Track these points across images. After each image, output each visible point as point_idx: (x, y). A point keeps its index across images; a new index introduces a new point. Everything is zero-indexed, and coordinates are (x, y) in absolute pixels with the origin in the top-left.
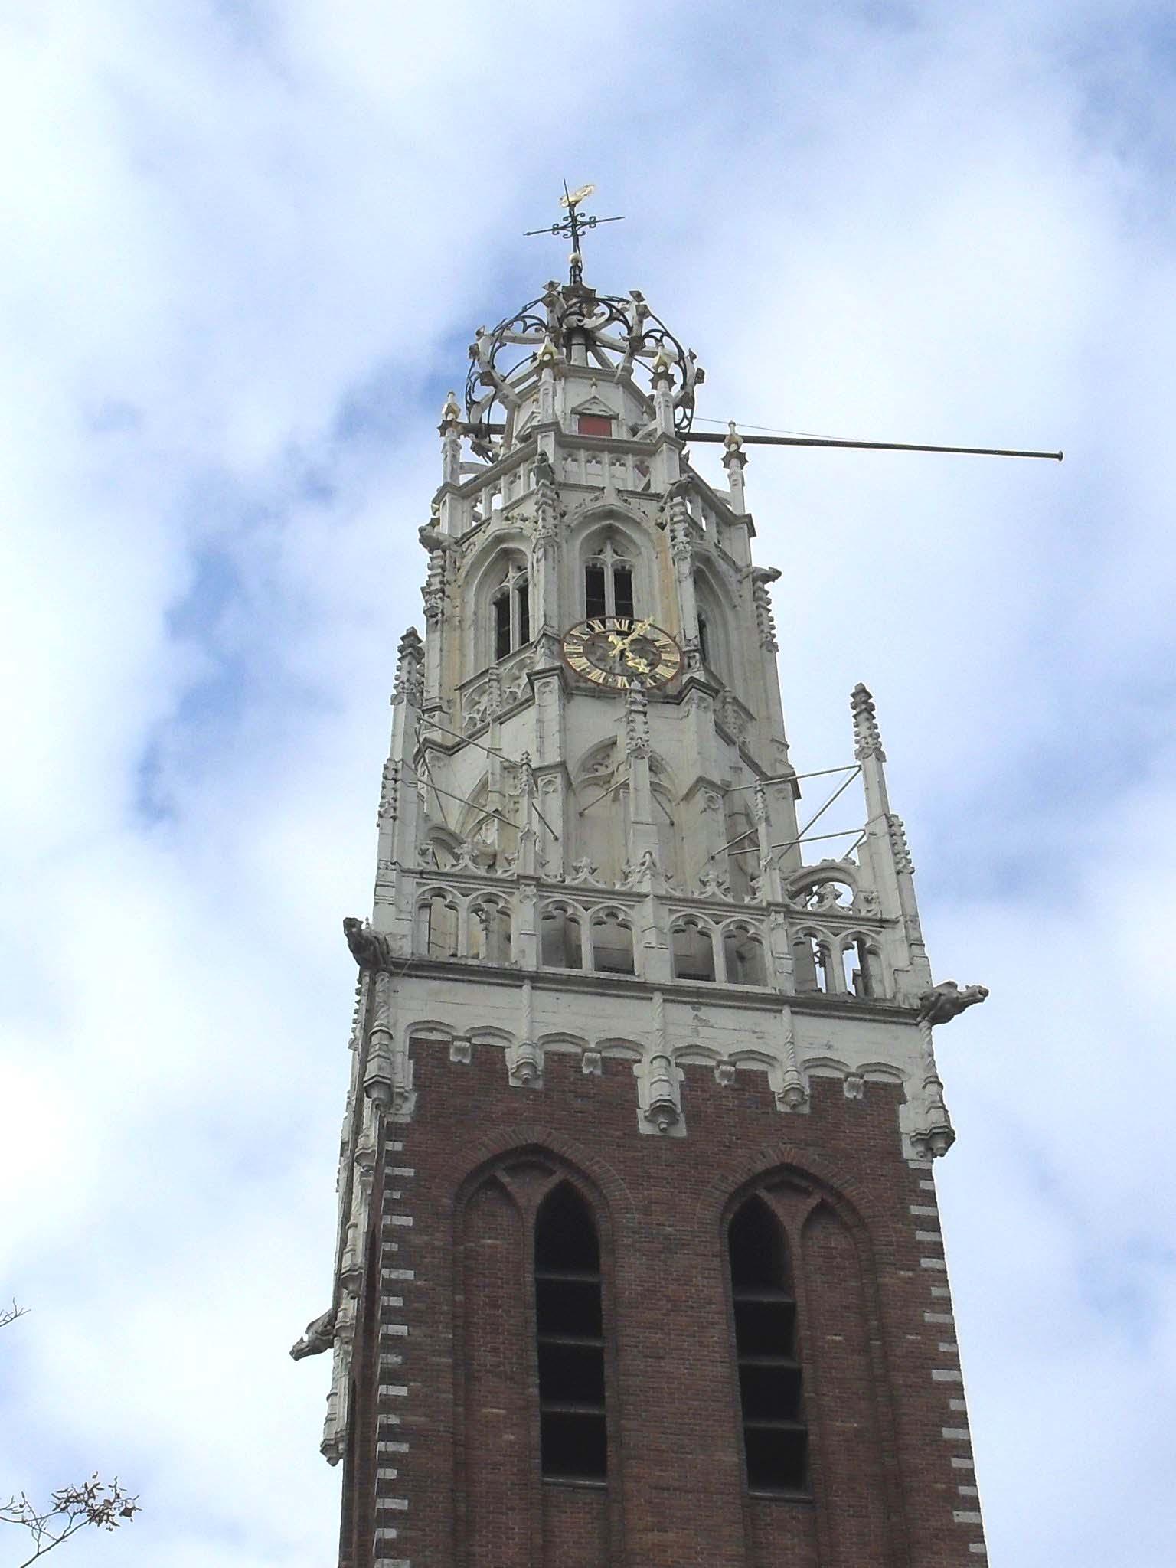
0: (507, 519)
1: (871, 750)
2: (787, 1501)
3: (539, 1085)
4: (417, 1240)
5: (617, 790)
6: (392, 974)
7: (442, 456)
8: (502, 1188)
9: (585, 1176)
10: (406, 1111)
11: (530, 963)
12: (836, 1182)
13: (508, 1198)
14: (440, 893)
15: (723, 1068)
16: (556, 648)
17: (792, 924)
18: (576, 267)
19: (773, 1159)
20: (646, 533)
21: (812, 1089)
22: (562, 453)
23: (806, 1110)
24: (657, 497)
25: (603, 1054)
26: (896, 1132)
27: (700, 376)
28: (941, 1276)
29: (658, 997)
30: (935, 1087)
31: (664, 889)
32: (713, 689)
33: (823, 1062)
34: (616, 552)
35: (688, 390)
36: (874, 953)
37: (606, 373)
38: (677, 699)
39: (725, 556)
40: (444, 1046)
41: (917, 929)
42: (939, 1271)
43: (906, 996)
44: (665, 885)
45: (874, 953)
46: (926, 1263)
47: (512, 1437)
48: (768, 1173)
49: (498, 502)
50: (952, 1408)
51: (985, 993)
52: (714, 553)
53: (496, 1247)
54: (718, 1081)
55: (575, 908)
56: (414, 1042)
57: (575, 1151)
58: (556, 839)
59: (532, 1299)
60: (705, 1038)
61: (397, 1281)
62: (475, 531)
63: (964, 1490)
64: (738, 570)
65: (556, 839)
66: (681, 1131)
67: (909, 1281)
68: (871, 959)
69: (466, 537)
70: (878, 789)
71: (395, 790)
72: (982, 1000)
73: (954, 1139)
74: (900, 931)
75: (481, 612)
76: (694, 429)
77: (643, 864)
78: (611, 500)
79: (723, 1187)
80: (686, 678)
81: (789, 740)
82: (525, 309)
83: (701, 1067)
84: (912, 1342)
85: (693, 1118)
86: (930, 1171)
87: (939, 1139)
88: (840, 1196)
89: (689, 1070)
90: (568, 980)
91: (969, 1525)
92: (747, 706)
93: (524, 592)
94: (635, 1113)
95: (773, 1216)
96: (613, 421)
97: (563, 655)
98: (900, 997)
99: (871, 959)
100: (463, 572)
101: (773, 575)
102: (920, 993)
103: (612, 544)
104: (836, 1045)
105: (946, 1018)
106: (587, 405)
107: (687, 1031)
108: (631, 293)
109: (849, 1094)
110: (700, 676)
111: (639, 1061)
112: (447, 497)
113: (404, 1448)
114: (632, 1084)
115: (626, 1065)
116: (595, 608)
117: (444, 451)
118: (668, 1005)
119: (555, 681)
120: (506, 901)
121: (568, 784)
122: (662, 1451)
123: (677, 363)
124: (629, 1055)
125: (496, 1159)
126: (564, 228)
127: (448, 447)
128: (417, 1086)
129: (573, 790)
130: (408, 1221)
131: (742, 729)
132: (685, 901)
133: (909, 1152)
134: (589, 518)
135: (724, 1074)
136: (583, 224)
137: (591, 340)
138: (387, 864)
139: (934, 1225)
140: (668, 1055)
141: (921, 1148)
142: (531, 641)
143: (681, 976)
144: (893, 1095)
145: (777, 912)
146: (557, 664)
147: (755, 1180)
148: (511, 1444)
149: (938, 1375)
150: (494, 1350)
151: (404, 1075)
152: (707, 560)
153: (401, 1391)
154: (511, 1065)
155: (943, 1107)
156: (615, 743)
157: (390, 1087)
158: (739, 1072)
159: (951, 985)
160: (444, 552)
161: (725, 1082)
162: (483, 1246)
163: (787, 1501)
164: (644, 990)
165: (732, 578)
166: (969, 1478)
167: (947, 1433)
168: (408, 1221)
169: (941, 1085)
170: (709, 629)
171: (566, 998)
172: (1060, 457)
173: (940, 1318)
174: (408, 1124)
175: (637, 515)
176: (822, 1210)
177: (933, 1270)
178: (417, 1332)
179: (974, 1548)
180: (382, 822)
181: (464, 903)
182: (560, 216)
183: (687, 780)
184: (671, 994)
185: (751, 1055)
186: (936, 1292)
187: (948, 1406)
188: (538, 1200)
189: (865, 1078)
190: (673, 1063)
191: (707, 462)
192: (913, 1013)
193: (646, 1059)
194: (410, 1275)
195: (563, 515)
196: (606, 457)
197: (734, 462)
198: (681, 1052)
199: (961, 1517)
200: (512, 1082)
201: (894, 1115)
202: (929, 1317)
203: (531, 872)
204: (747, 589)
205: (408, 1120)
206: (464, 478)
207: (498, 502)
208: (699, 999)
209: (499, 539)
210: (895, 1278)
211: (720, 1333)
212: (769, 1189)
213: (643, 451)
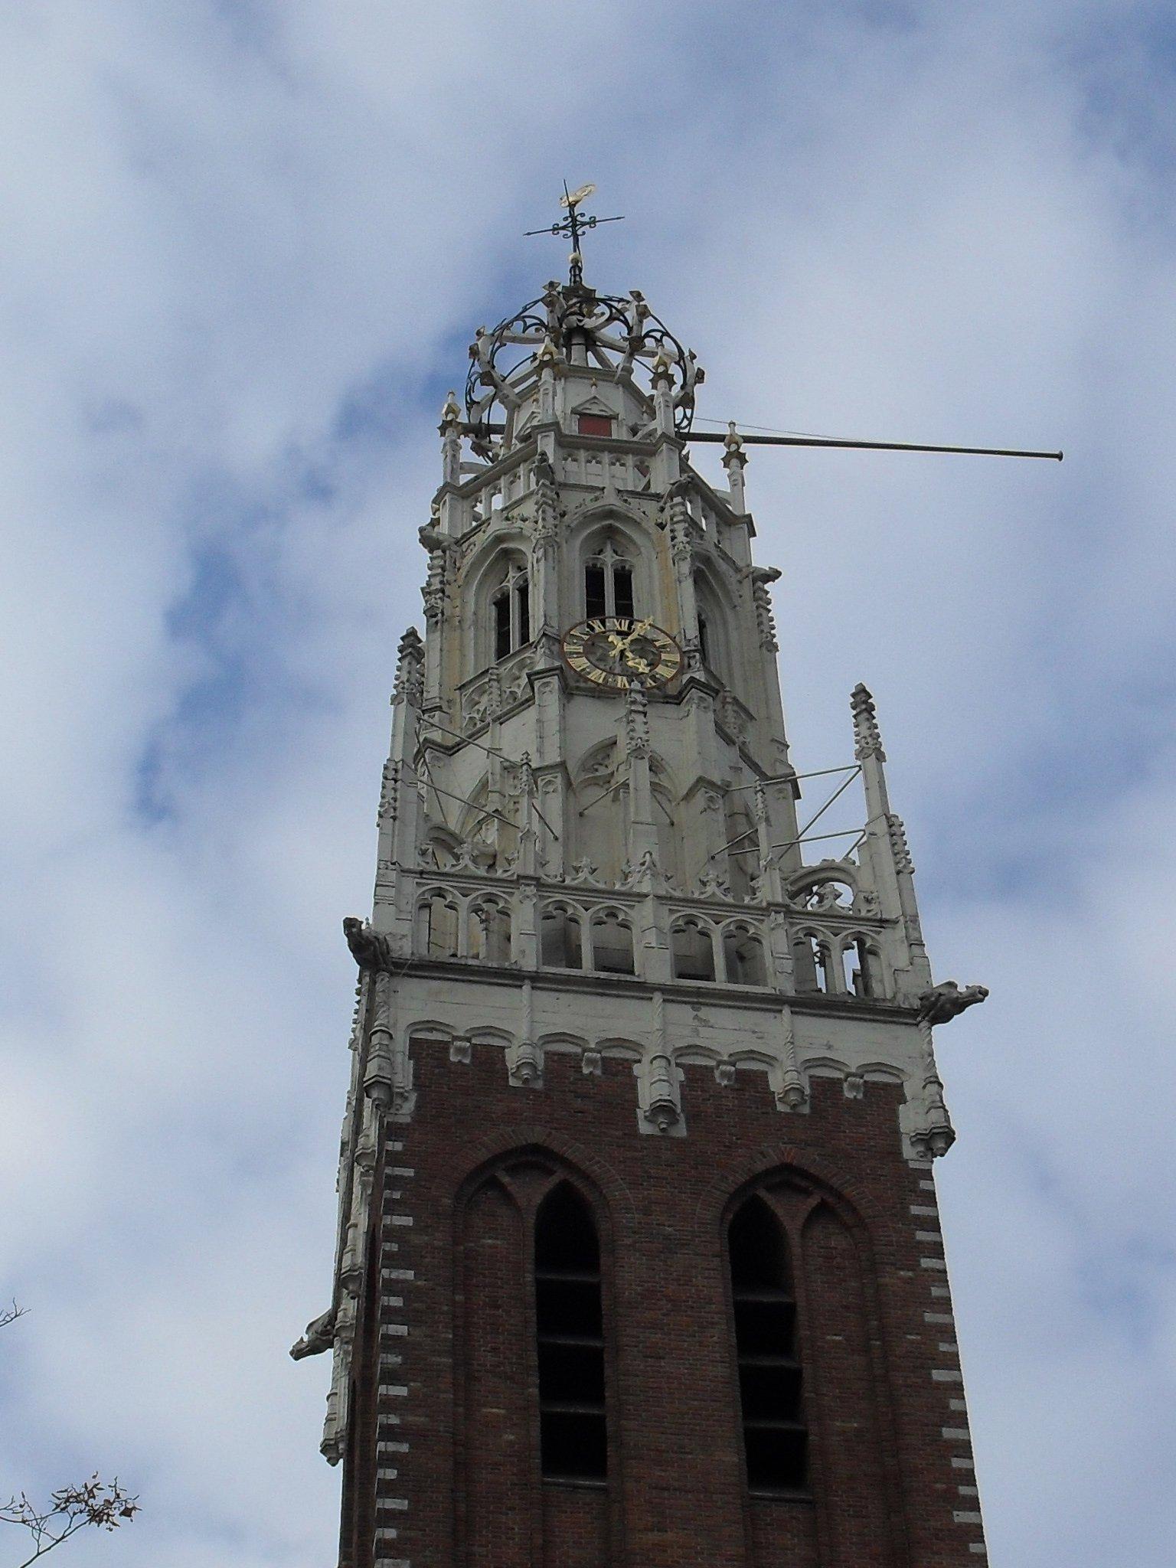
3: (539, 1085)
4: (416, 1240)
5: (617, 790)
6: (392, 974)
7: (442, 456)
8: (501, 1188)
9: (586, 1176)
10: (406, 1111)
11: (530, 963)
12: (835, 1182)
13: (508, 1198)
14: (440, 893)
15: (723, 1068)
16: (556, 648)
17: (792, 924)
18: (576, 267)
19: (774, 1159)
20: (646, 533)
23: (806, 1110)
24: (657, 497)
26: (896, 1132)
27: (700, 376)
28: (941, 1275)
29: (658, 997)
32: (713, 689)
33: (823, 1062)
34: (616, 552)
35: (688, 389)
37: (606, 373)
38: (677, 699)
39: (725, 557)
40: (444, 1047)
41: (918, 929)
42: (939, 1271)
43: (906, 997)
45: (874, 953)
46: (926, 1263)
49: (498, 502)
51: (985, 993)
52: (714, 553)
54: (718, 1081)
55: (575, 908)
57: (575, 1151)
58: (556, 839)
59: (532, 1299)
60: (705, 1038)
61: (397, 1281)
62: (475, 531)
63: (963, 1490)
64: (738, 570)
65: (556, 839)
66: (681, 1131)
68: (870, 959)
69: (466, 537)
70: (878, 789)
71: (395, 790)
72: (982, 1000)
73: (954, 1139)
74: (900, 931)
76: (694, 429)
77: (643, 864)
78: (611, 500)
80: (686, 678)
81: (789, 743)
82: (525, 309)
84: (912, 1342)
85: (693, 1118)
86: (929, 1171)
87: (940, 1138)
88: (839, 1196)
89: (689, 1069)
90: (568, 980)
93: (524, 592)
95: (774, 1215)
96: (613, 421)
97: (563, 655)
98: (900, 997)
99: (870, 959)
100: (463, 572)
101: (773, 575)
102: (920, 992)
105: (946, 1018)
108: (631, 293)
109: (849, 1094)
110: (700, 676)
111: (639, 1061)
112: (447, 497)
113: (404, 1448)
114: (632, 1084)
115: (626, 1065)
116: (595, 608)
117: (444, 451)
118: (669, 1005)
119: (555, 681)
120: (506, 901)
121: (568, 784)
123: (677, 363)
124: (629, 1055)
126: (564, 228)
127: (448, 447)
128: (417, 1086)
130: (408, 1221)
131: (742, 729)
133: (909, 1151)
135: (724, 1074)
136: (583, 224)
137: (590, 340)
138: (387, 864)
139: (934, 1225)
140: (668, 1055)
142: (531, 641)
143: (681, 976)
144: (893, 1095)
145: (777, 912)
146: (557, 664)
147: (755, 1180)
148: (511, 1444)
149: (938, 1375)
151: (404, 1075)
152: (707, 560)
153: (401, 1391)
155: (943, 1107)
156: (615, 743)
157: (389, 1087)
158: (739, 1072)
159: (951, 985)
160: (444, 552)
162: (483, 1246)
164: (643, 990)
165: (732, 578)
166: (969, 1478)
167: (948, 1433)
168: (408, 1221)
169: (941, 1085)
172: (1060, 457)
175: (636, 515)
176: (822, 1211)
177: (933, 1270)
179: (974, 1548)
181: (464, 903)
182: (560, 216)
184: (672, 994)
185: (751, 1055)
186: (936, 1292)
188: (538, 1199)
189: (865, 1078)
190: (673, 1062)
192: (913, 1013)
193: (646, 1059)
194: (410, 1275)
195: (563, 515)
197: (734, 462)
198: (681, 1052)
199: (961, 1517)
200: (512, 1082)
201: (894, 1116)
202: (929, 1317)
203: (531, 872)
204: (747, 590)
205: (408, 1120)
206: (464, 478)
207: (498, 502)
208: (699, 999)
209: (499, 539)
211: (720, 1333)
212: (769, 1189)
213: (643, 451)
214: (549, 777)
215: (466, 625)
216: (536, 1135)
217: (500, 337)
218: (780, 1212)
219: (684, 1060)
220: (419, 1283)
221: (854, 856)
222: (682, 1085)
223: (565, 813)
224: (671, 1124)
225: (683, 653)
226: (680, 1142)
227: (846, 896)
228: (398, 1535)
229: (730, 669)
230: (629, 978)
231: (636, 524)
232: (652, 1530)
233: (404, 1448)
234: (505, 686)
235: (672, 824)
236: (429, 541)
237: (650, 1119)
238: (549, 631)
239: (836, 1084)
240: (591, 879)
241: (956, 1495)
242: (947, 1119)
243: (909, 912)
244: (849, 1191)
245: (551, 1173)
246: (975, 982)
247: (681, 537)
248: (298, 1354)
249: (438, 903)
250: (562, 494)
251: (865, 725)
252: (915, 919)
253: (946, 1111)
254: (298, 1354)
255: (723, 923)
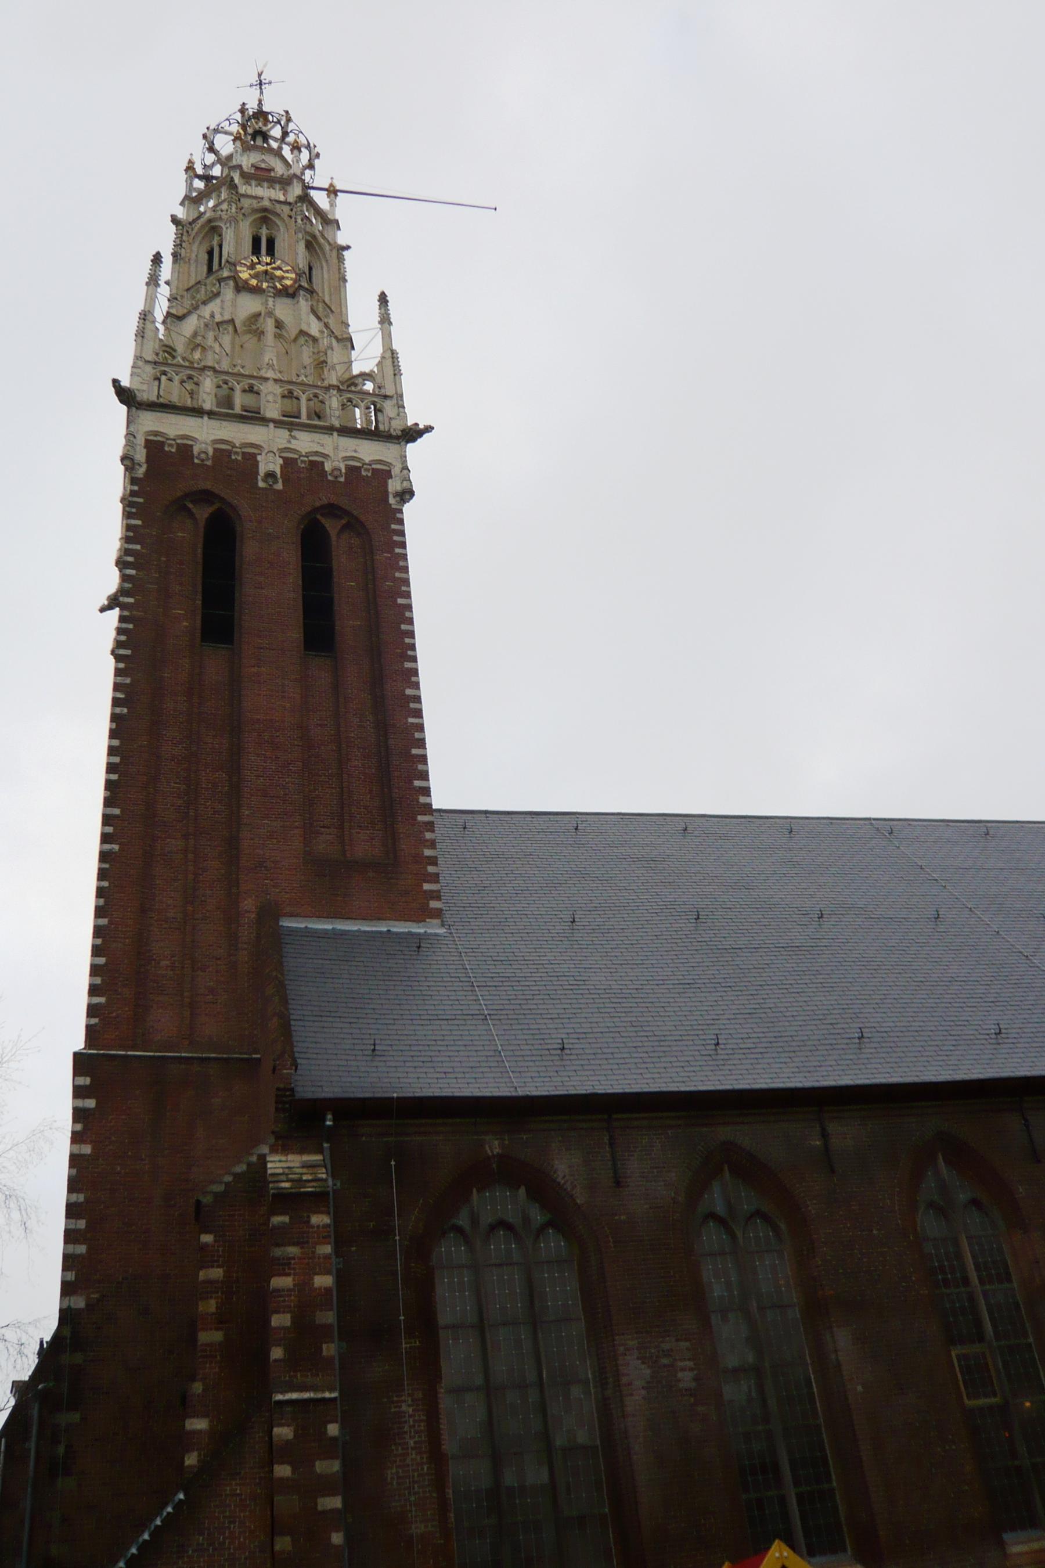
0: (214, 211)
1: (385, 320)
2: (323, 656)
3: (209, 463)
5: (260, 334)
6: (137, 408)
7: (185, 184)
8: (189, 510)
9: (231, 506)
10: (141, 472)
11: (207, 406)
12: (355, 513)
13: (191, 515)
14: (164, 373)
15: (302, 458)
16: (233, 268)
17: (341, 396)
18: (260, 102)
19: (325, 501)
21: (346, 470)
22: (242, 181)
23: (342, 479)
24: (290, 204)
25: (243, 450)
27: (318, 155)
28: (404, 557)
29: (271, 425)
30: (407, 471)
31: (279, 376)
32: (311, 292)
33: (353, 458)
34: (268, 229)
35: (312, 161)
36: (380, 411)
37: (270, 150)
38: (293, 296)
39: (323, 236)
40: (162, 444)
41: (402, 400)
42: (404, 554)
43: (395, 430)
44: (279, 375)
45: (380, 411)
46: (397, 550)
47: (187, 624)
48: (323, 507)
49: (211, 204)
50: (407, 615)
51: (433, 428)
52: (318, 234)
53: (184, 537)
54: (299, 465)
55: (233, 382)
56: (147, 441)
58: (227, 354)
59: (200, 561)
60: (294, 445)
61: (132, 550)
62: (198, 218)
63: (410, 653)
64: (330, 244)
65: (227, 354)
66: (279, 486)
67: (389, 558)
68: (379, 414)
69: (194, 221)
70: (387, 337)
71: (144, 324)
72: (431, 431)
73: (414, 495)
74: (394, 401)
75: (200, 256)
76: (315, 185)
78: (266, 203)
79: (299, 512)
81: (350, 323)
82: (230, 116)
83: (291, 458)
84: (388, 586)
85: (286, 480)
86: (402, 510)
87: (407, 494)
88: (356, 518)
89: (285, 459)
90: (227, 415)
91: (411, 669)
92: (330, 306)
93: (221, 246)
94: (257, 478)
95: (323, 527)
97: (237, 272)
98: (392, 430)
99: (379, 414)
100: (192, 237)
101: (348, 248)
102: (401, 428)
103: (266, 225)
104: (359, 451)
105: (413, 439)
106: (260, 163)
107: (285, 441)
108: (284, 111)
109: (364, 473)
111: (261, 454)
113: (131, 626)
114: (256, 464)
115: (254, 456)
117: (186, 181)
118: (276, 429)
119: (231, 283)
121: (236, 331)
122: (261, 631)
123: (306, 148)
125: (186, 495)
126: (256, 85)
128: (147, 462)
129: (238, 335)
130: (139, 522)
131: (327, 316)
132: (290, 382)
133: (392, 500)
134: (255, 211)
135: (302, 462)
136: (265, 84)
137: (265, 137)
138: (138, 357)
139: (402, 533)
140: (275, 451)
141: (398, 499)
143: (284, 416)
144: (388, 474)
145: (333, 389)
146: (232, 274)
147: (316, 510)
148: (186, 627)
149: (400, 601)
150: (181, 584)
151: (141, 455)
152: (314, 237)
153: (131, 600)
154: (195, 453)
155: (410, 480)
157: (132, 460)
158: (310, 461)
159: (417, 424)
160: (183, 227)
161: (303, 465)
162: (178, 537)
163: (323, 656)
164: (264, 421)
165: (327, 248)
166: (413, 647)
167: (403, 627)
168: (139, 522)
169: (409, 471)
170: (314, 272)
171: (225, 423)
173: (403, 575)
174: (141, 478)
175: (278, 211)
176: (347, 527)
177: (401, 554)
178: (141, 573)
179: (413, 679)
180: (138, 340)
181: (177, 379)
182: (254, 79)
183: (294, 333)
184: (278, 424)
185: (316, 453)
186: (401, 563)
187: (404, 615)
188: (206, 515)
190: (277, 456)
191: (321, 199)
192: (398, 438)
193: (263, 454)
194: (138, 547)
195: (241, 209)
196: (265, 184)
198: (281, 450)
199: (408, 665)
200: (196, 461)
201: (386, 485)
202: (397, 575)
204: (334, 253)
205: (142, 476)
206: (194, 194)
207: (211, 204)
208: (291, 427)
209: (210, 221)
210: (381, 557)
212: (322, 515)
213: (284, 183)
214: (225, 326)
215: (192, 262)
216: (207, 485)
217: (216, 131)
218: (327, 526)
219: (283, 455)
220: (144, 551)
221: (375, 370)
222: (281, 466)
223: (233, 343)
224: (274, 483)
225: (296, 274)
226: (278, 491)
227: (369, 386)
228: (125, 666)
229: (323, 289)
230: (257, 415)
231: (278, 215)
232: (254, 666)
233: (131, 626)
234: (208, 288)
235: (287, 353)
236: (175, 220)
237: (265, 480)
238: (230, 260)
239: (358, 469)
240: (241, 370)
241: (407, 655)
242: (412, 486)
243: (399, 392)
244: (362, 518)
245: (213, 503)
246: (428, 424)
247: (299, 221)
248: (103, 610)
249: (163, 378)
250: (242, 200)
251: (383, 310)
252: (401, 396)
253: (411, 482)
254: (103, 610)
255: (307, 393)
